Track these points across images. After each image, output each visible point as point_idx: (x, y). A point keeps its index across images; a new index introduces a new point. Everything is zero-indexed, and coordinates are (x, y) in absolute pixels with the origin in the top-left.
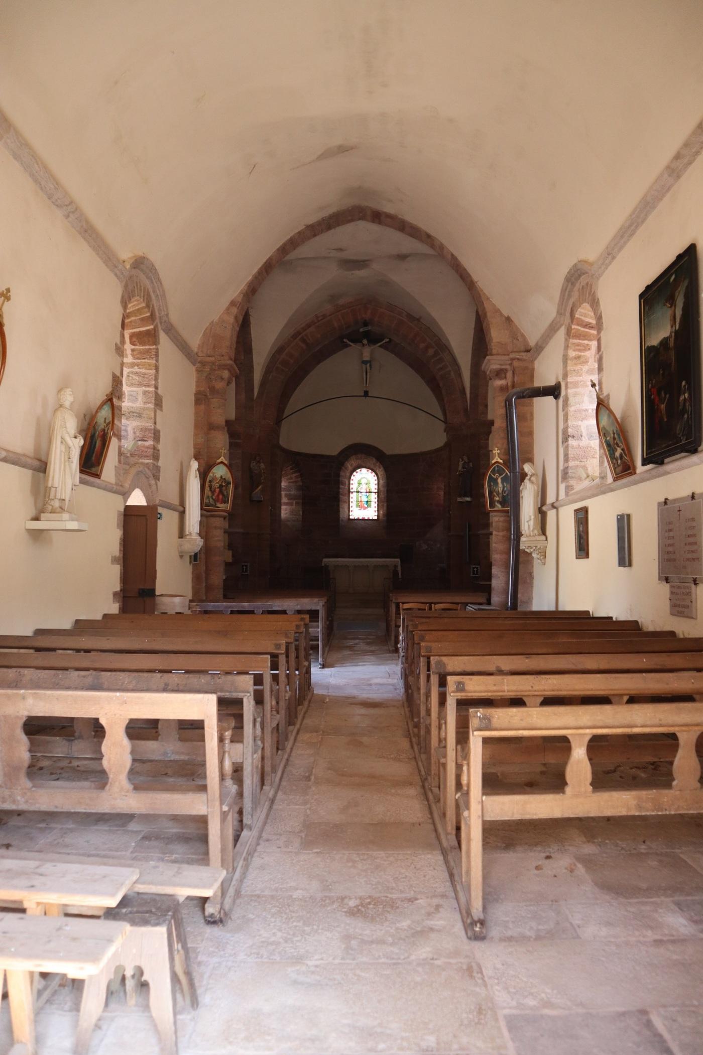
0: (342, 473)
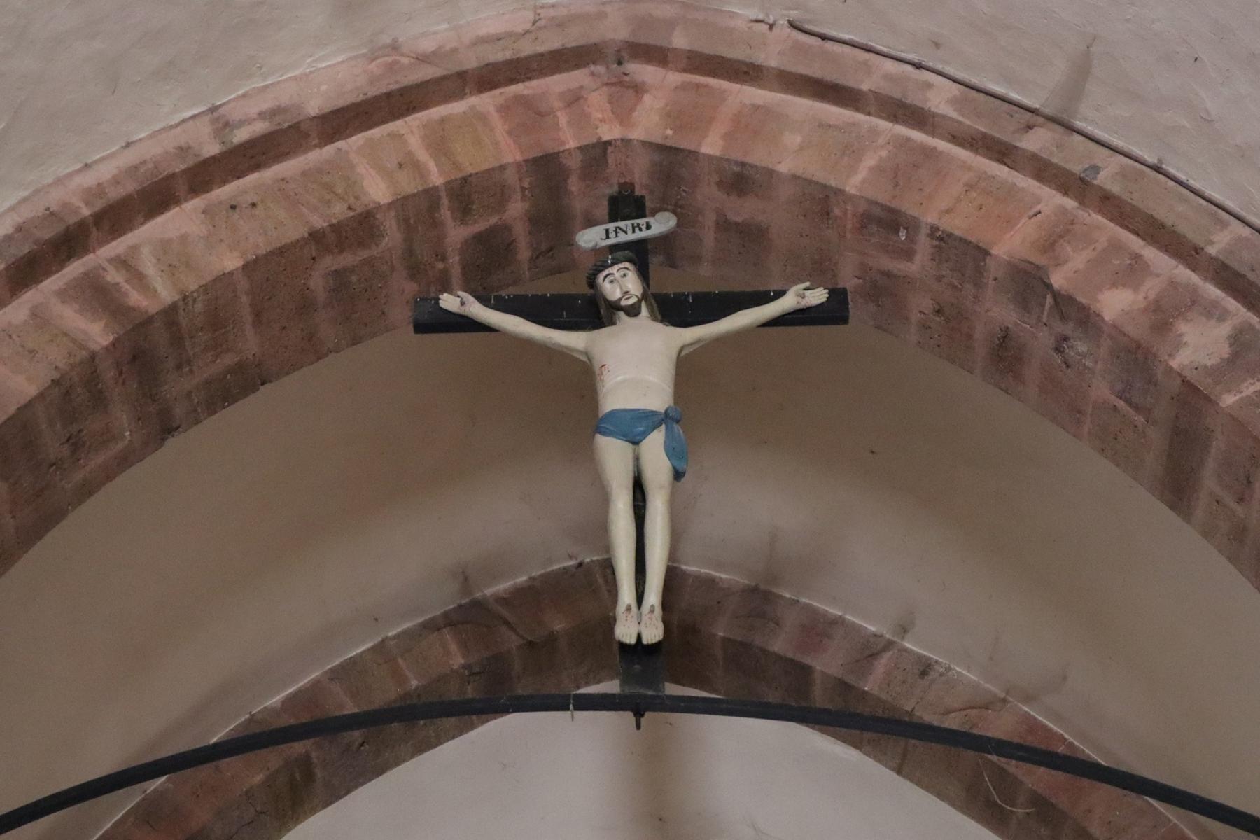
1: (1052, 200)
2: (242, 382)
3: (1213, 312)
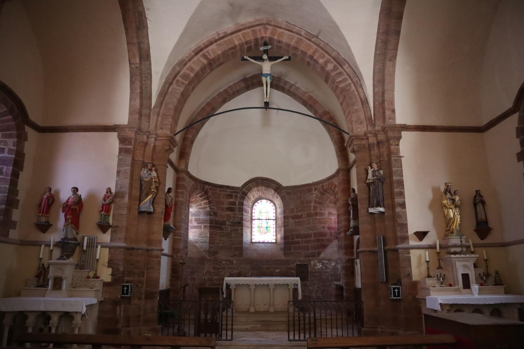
0: (245, 202)
1: (315, 47)
2: (221, 64)
3: (332, 62)
